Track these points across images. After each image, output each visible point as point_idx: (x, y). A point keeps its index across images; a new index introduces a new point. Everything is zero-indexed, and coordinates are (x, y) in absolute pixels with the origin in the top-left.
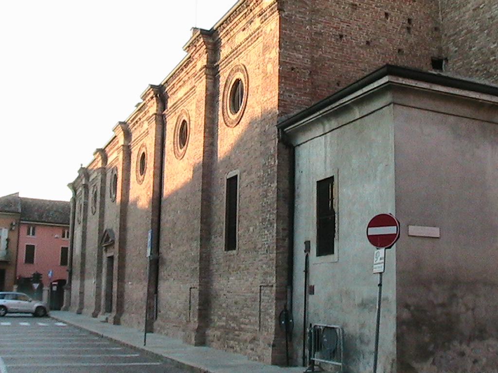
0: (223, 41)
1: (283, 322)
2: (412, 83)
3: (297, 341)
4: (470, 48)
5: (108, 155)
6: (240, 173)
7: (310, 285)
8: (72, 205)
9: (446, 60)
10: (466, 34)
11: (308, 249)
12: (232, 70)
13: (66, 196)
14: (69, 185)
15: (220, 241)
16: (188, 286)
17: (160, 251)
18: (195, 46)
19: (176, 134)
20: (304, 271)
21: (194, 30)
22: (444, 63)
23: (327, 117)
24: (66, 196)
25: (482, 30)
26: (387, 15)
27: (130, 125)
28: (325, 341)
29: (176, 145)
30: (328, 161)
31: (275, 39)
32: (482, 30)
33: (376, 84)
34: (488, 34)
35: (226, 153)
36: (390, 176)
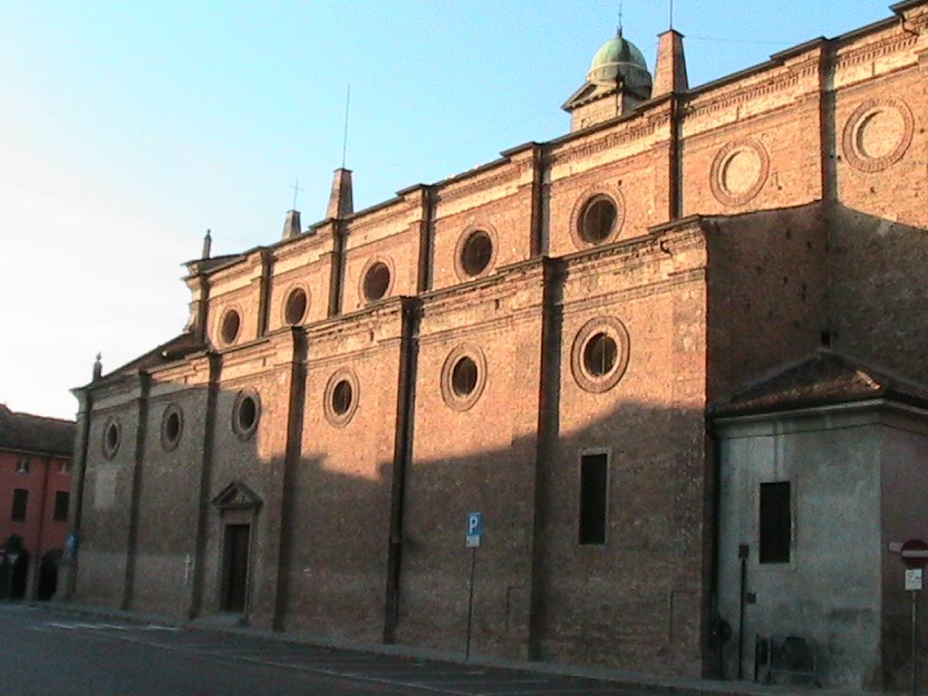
0: (571, 277)
1: (714, 633)
2: (905, 407)
3: (300, 667)
4: (870, 329)
5: (225, 364)
6: (613, 453)
7: (748, 592)
8: (81, 431)
9: (836, 335)
10: (864, 311)
11: (744, 551)
12: (593, 319)
13: (68, 410)
14: (76, 391)
15: (566, 532)
16: (506, 584)
17: (404, 530)
18: (524, 273)
19: (446, 373)
20: (415, 547)
21: (343, 174)
22: (832, 338)
23: (784, 420)
24: (68, 410)
25: (887, 313)
26: (786, 280)
27: (311, 335)
28: (796, 656)
29: (445, 388)
30: (780, 464)
31: (699, 312)
32: (887, 313)
33: (865, 404)
34: (894, 319)
35: (578, 422)
36: (875, 494)
